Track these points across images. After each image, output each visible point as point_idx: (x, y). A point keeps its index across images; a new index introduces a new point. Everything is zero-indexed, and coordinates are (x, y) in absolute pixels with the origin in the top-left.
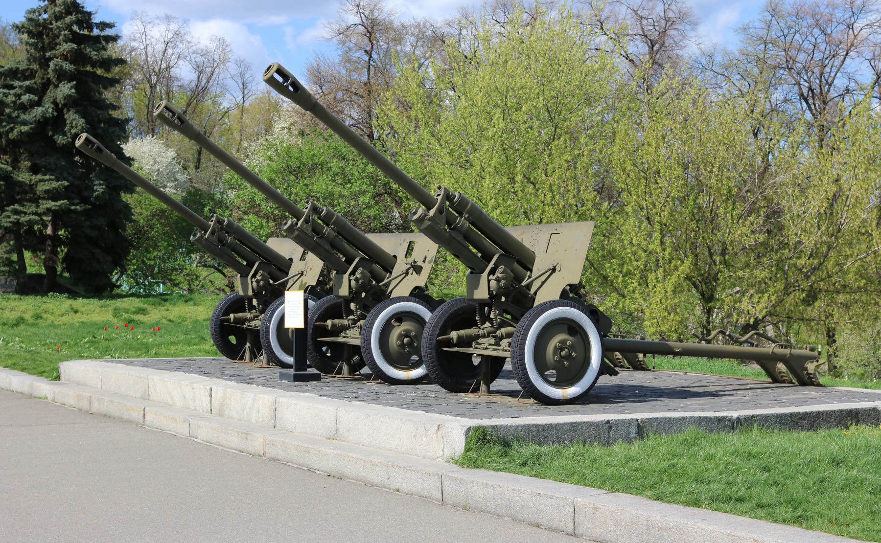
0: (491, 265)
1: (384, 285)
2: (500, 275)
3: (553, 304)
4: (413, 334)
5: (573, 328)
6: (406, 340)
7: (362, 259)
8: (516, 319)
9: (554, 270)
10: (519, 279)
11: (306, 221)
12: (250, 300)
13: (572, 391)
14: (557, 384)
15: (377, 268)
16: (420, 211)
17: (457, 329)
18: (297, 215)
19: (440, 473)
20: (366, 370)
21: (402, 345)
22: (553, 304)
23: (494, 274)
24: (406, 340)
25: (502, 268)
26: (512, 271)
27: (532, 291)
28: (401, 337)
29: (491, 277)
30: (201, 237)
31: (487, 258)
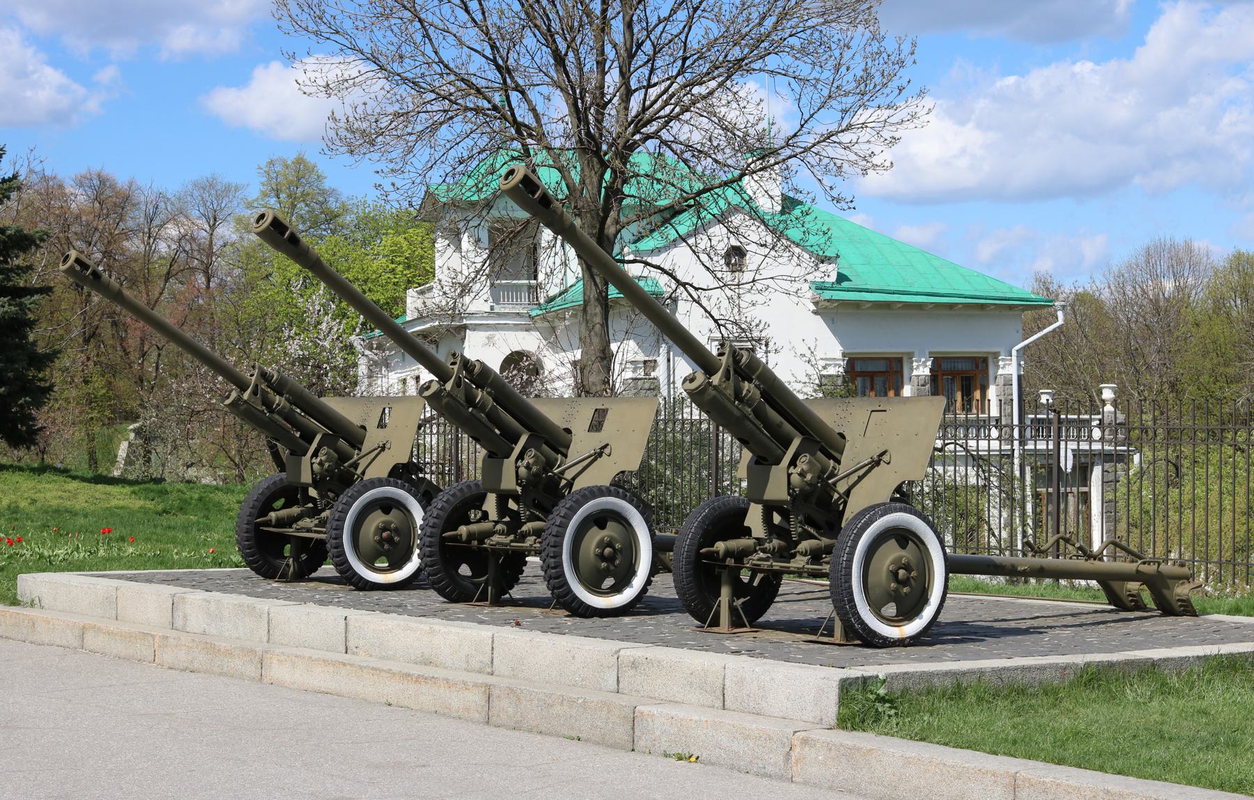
0: (518, 449)
1: (351, 466)
2: (531, 461)
3: (379, 483)
4: (618, 546)
5: (903, 536)
6: (608, 550)
7: (325, 435)
8: (547, 511)
9: (383, 448)
10: (550, 464)
11: (255, 393)
12: (305, 489)
13: (628, 594)
14: (617, 589)
15: (342, 443)
16: (234, 395)
17: (724, 540)
18: (242, 387)
19: (487, 729)
20: (328, 569)
21: (601, 557)
22: (379, 483)
23: (795, 466)
24: (608, 550)
25: (324, 450)
26: (336, 451)
27: (359, 471)
28: (602, 544)
29: (792, 470)
30: (239, 398)
31: (308, 437)
